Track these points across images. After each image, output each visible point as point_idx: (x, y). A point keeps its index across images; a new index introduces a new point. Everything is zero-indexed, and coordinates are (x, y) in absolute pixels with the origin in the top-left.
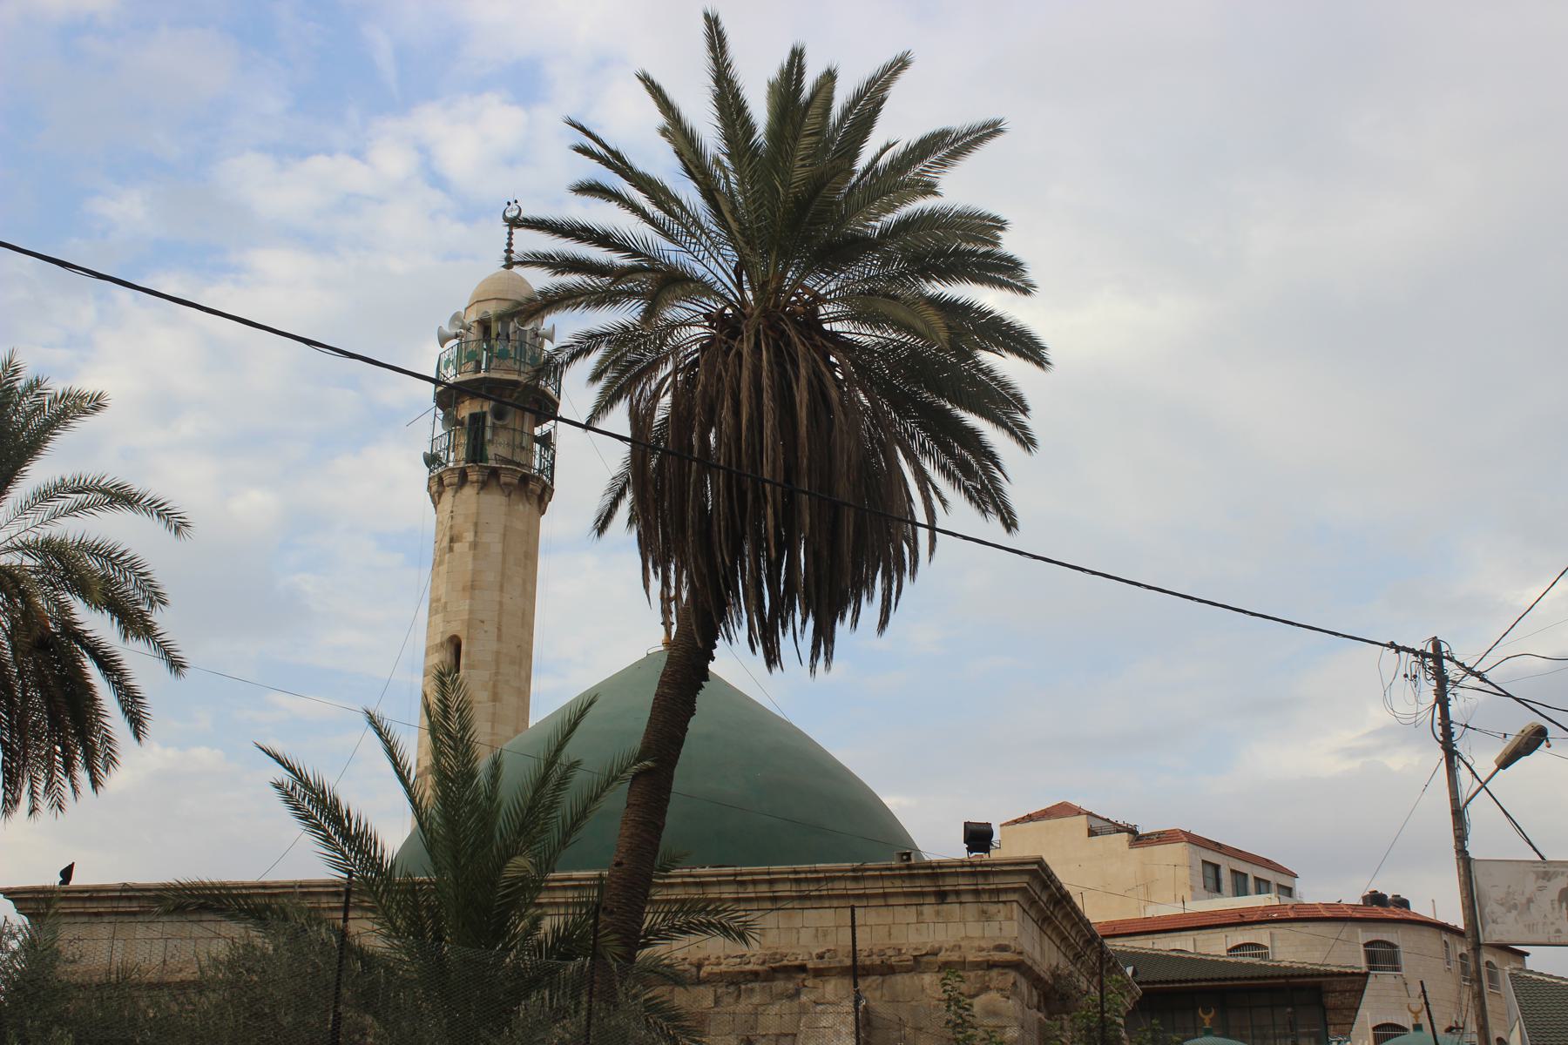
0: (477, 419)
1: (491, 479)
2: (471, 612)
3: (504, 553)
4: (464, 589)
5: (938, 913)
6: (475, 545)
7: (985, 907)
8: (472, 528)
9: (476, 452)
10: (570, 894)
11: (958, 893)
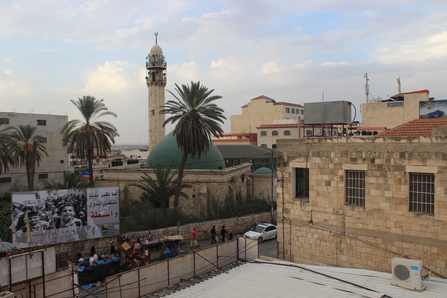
6: (155, 95)
9: (154, 79)
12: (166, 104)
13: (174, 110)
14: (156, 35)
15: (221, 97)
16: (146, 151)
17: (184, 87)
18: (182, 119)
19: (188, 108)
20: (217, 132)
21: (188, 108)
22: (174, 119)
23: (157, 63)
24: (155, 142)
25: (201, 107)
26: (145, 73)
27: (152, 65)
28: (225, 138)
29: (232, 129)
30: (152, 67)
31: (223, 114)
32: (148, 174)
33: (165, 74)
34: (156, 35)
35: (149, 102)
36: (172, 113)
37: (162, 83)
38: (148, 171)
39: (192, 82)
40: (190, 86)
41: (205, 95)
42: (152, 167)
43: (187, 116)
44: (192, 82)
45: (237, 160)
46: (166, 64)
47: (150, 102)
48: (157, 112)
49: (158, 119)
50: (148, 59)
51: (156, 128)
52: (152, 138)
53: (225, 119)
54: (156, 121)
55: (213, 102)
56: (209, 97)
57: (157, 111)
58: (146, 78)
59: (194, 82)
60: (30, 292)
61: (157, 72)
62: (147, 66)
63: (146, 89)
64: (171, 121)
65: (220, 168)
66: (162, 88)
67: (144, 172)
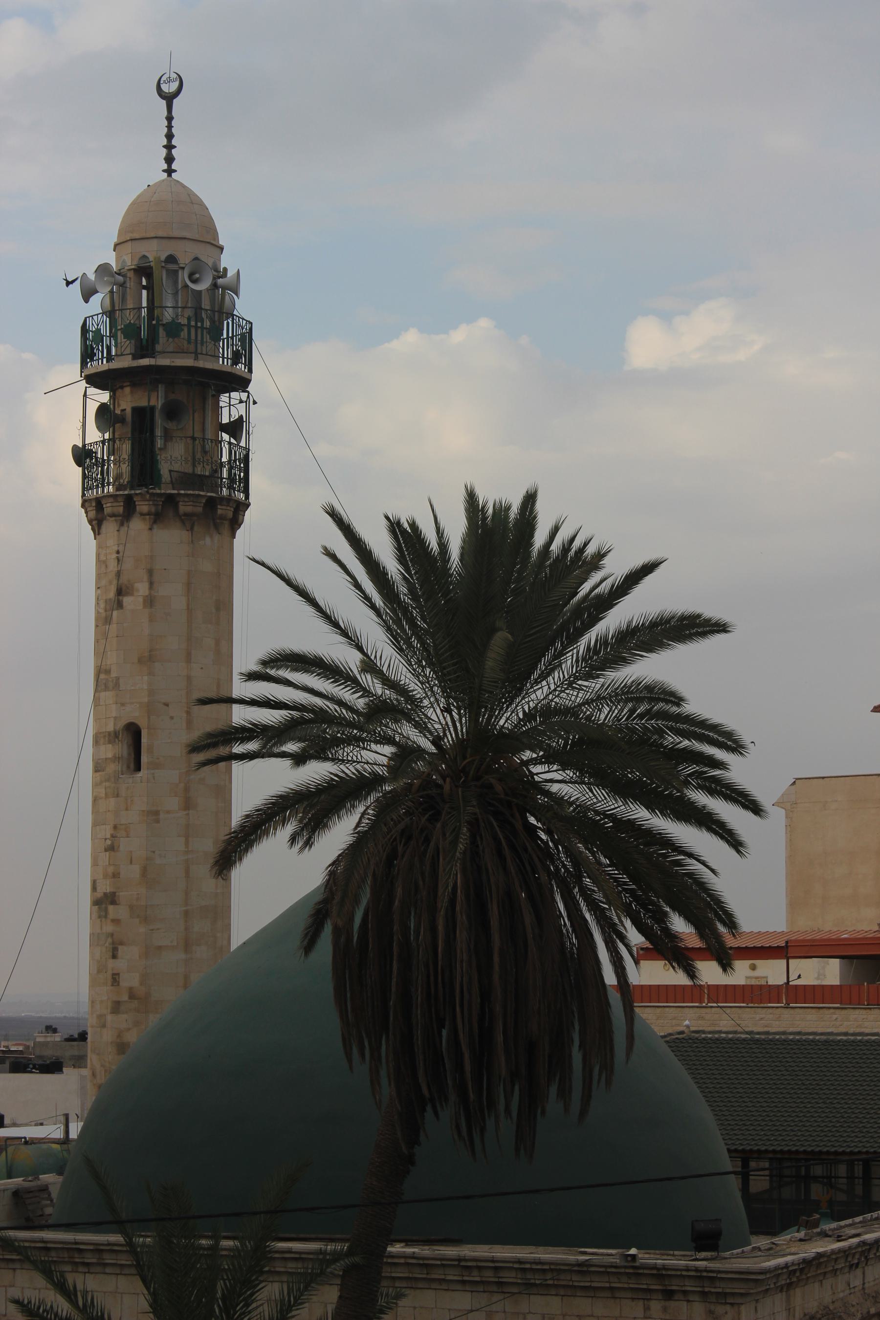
0: (143, 417)
1: (165, 510)
2: (151, 692)
3: (189, 610)
4: (140, 661)
5: (665, 1309)
6: (150, 601)
7: (712, 1307)
8: (145, 578)
9: (144, 469)
10: (291, 1265)
11: (685, 1292)
12: (252, 676)
13: (310, 731)
14: (170, 99)
15: (720, 628)
16: (53, 1067)
17: (406, 537)
18: (384, 808)
19: (435, 716)
20: (679, 925)
21: (441, 718)
22: (310, 810)
23: (173, 330)
24: (139, 1000)
25: (547, 712)
26: (66, 413)
27: (128, 346)
28: (742, 973)
29: (799, 892)
30: (126, 362)
31: (738, 771)
32: (77, 1280)
33: (236, 428)
34: (170, 99)
35: (100, 653)
36: (299, 759)
37: (212, 504)
38: (75, 1249)
39: (471, 497)
40: (456, 529)
41: (578, 611)
42: (117, 1224)
43: (427, 783)
44: (471, 497)
45: (842, 1170)
46: (247, 339)
47: (112, 659)
48: (168, 740)
49: (174, 803)
50: (96, 303)
51: (149, 875)
52: (120, 965)
53: (755, 808)
54: (153, 815)
55: (649, 668)
56: (612, 621)
57: (163, 731)
58: (82, 455)
59: (488, 497)
60: (531, 1269)
61: (173, 412)
62: (87, 355)
63: (77, 547)
64: (290, 828)
65: (707, 1240)
66: (209, 542)
67: (47, 1264)
